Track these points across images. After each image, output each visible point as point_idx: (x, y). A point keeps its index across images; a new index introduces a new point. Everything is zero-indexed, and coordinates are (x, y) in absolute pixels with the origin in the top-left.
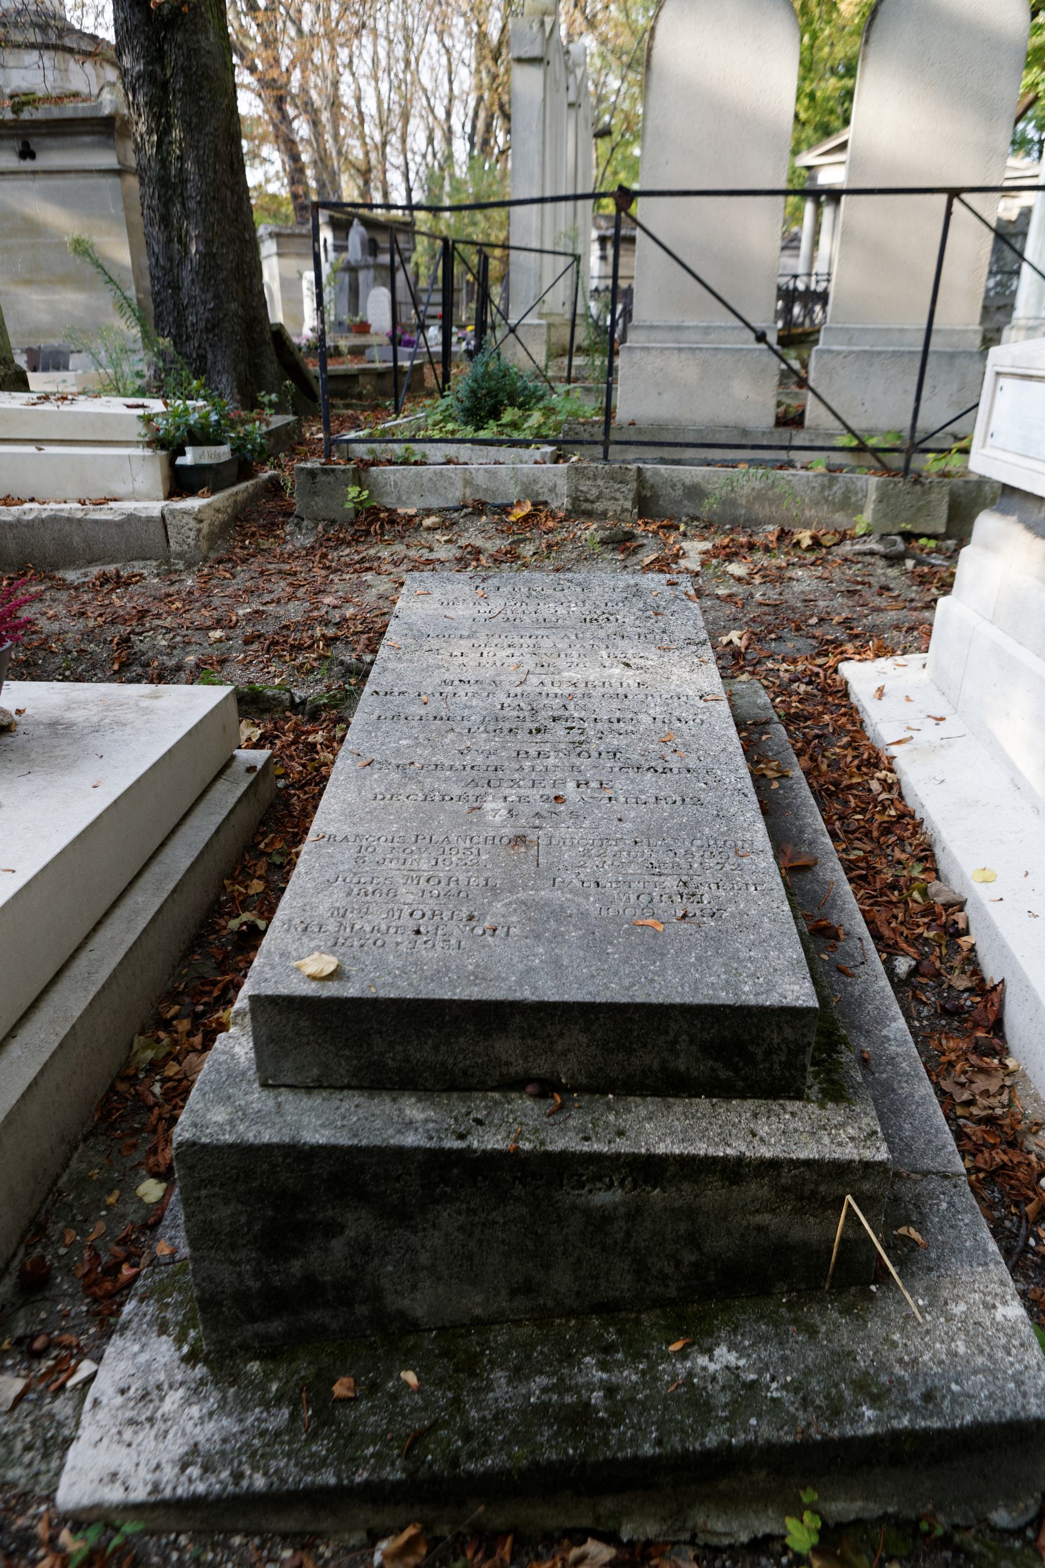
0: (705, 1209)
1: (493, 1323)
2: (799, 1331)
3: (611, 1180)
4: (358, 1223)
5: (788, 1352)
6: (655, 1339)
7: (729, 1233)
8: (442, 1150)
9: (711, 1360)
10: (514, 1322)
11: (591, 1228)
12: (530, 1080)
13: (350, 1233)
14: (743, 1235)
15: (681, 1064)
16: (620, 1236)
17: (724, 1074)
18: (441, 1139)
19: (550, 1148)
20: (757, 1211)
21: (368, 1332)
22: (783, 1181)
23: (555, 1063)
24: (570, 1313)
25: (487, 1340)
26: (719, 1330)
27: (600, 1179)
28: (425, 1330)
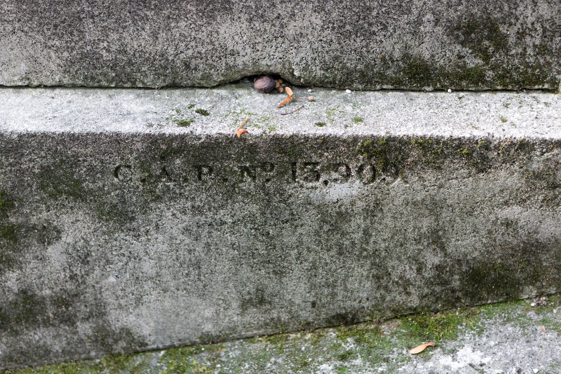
0: (449, 202)
1: (224, 341)
2: (548, 329)
3: (348, 169)
4: (76, 226)
5: (536, 349)
6: (395, 345)
7: (475, 230)
8: (162, 136)
9: (454, 360)
10: (247, 338)
11: (326, 228)
12: (258, 75)
13: (67, 238)
14: (490, 232)
15: (425, 51)
16: (358, 236)
17: (473, 62)
18: (161, 126)
19: (280, 132)
20: (506, 203)
21: (93, 354)
22: (535, 166)
23: (286, 51)
24: (307, 327)
25: (218, 356)
26: (463, 333)
27: (335, 167)
28: (153, 350)
